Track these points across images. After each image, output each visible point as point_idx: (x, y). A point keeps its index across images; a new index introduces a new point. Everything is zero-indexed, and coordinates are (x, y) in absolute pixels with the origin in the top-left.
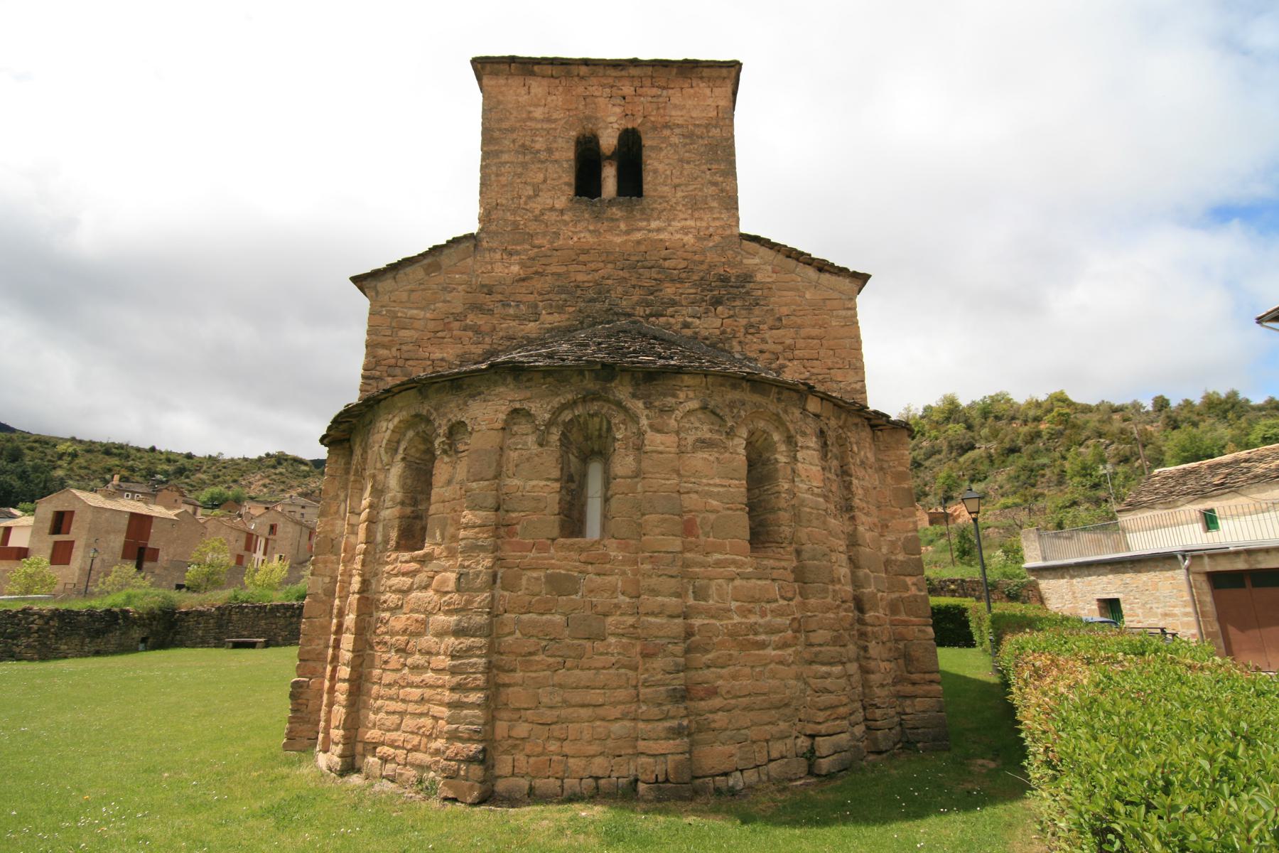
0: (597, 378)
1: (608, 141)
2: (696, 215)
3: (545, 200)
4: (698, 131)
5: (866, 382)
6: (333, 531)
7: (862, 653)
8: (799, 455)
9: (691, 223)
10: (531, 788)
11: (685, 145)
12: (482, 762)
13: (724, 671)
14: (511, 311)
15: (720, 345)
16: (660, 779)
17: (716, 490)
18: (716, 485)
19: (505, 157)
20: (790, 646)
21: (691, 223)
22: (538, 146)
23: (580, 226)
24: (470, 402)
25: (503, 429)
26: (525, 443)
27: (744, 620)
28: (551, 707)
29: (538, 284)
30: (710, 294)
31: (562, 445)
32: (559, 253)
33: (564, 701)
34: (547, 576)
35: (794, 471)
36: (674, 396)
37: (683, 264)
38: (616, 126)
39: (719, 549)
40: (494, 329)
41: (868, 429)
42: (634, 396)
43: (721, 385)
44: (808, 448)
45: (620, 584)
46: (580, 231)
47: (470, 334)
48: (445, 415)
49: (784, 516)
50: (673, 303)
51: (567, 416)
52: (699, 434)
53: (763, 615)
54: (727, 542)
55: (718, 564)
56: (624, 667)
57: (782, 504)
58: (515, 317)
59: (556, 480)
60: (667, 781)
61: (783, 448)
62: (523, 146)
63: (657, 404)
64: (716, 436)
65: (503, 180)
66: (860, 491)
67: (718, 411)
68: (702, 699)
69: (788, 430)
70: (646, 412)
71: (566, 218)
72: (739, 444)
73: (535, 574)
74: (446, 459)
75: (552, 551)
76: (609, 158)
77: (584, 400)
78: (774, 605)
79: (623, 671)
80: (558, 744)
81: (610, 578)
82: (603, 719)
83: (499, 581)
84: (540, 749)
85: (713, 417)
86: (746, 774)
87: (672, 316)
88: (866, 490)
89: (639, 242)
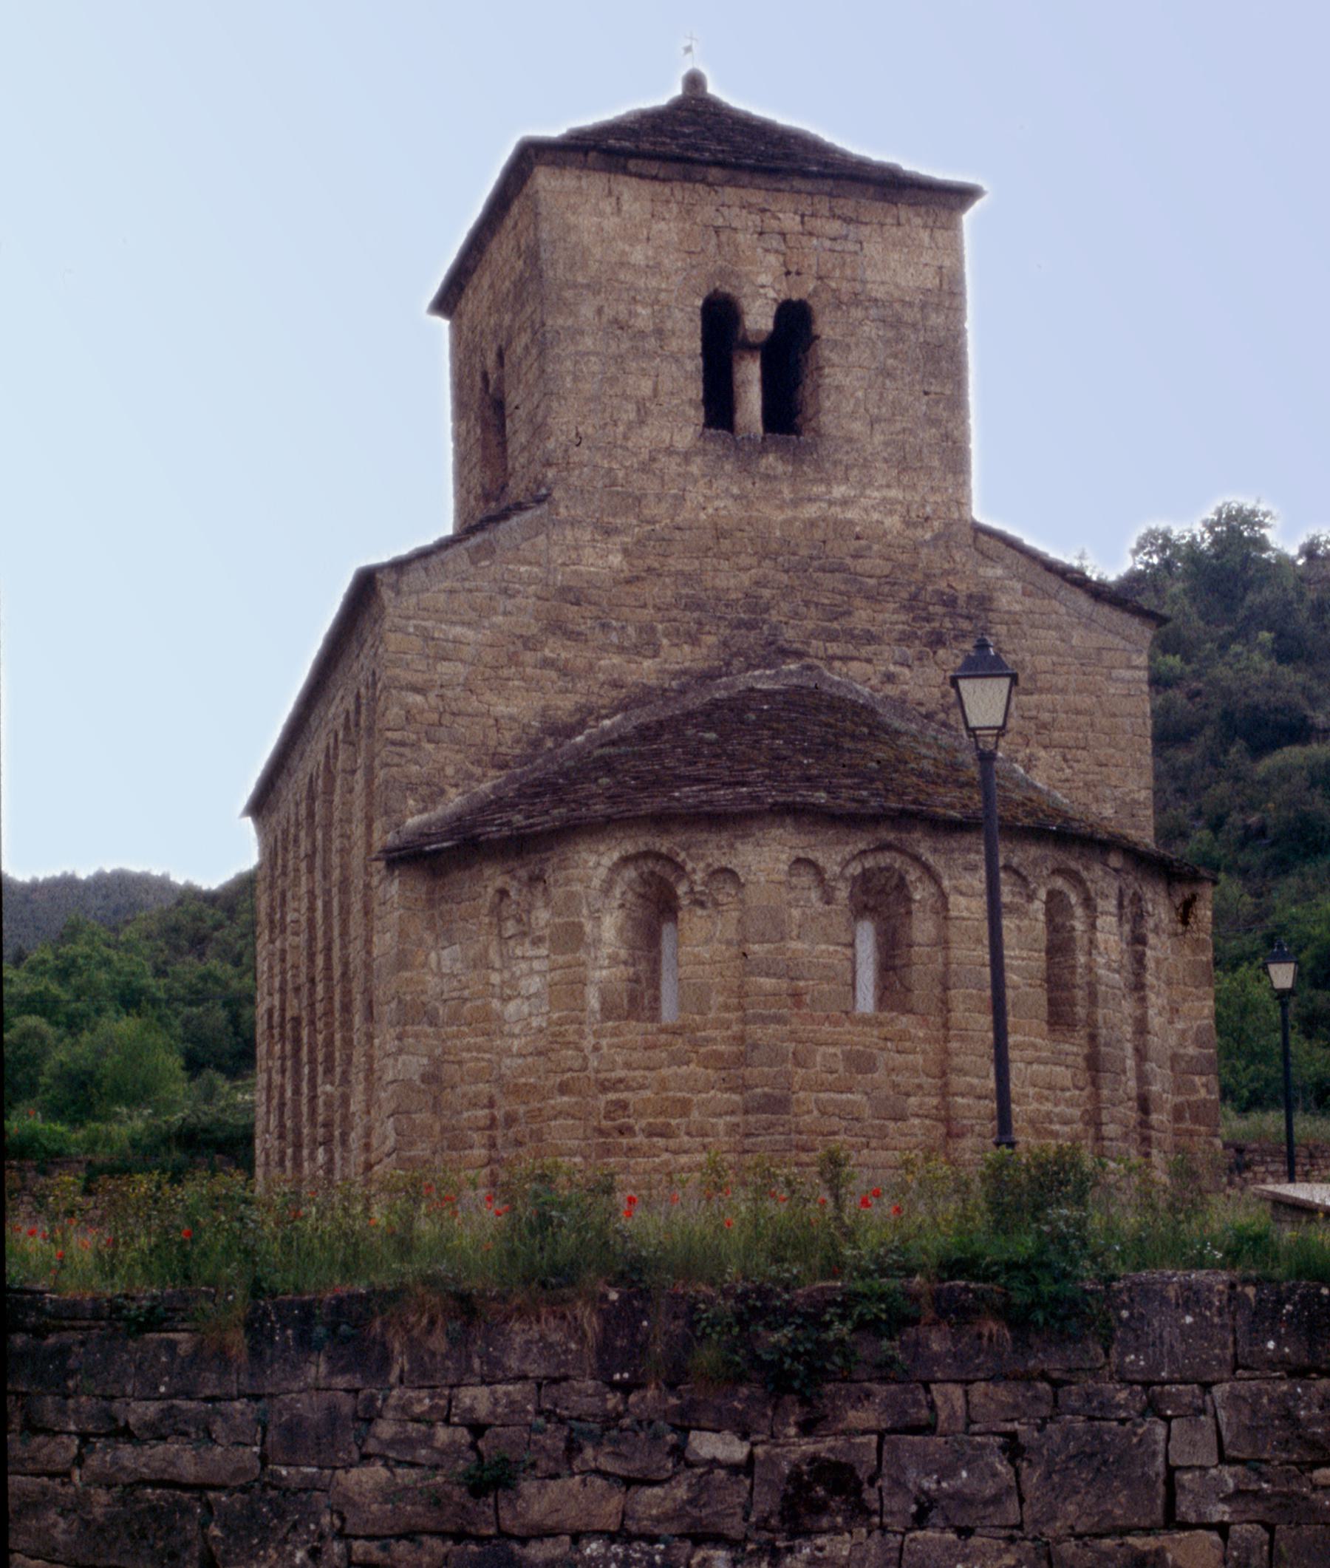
1: (759, 318)
2: (905, 479)
3: (648, 436)
4: (911, 315)
6: (424, 992)
8: (1099, 923)
9: (894, 493)
11: (887, 342)
14: (614, 638)
19: (588, 342)
21: (894, 493)
22: (639, 323)
23: (721, 483)
24: (738, 845)
26: (808, 900)
29: (653, 591)
30: (928, 627)
32: (687, 535)
35: (1091, 942)
37: (886, 568)
38: (772, 294)
40: (591, 666)
42: (935, 851)
46: (712, 494)
47: (554, 675)
48: (702, 857)
50: (871, 638)
51: (855, 869)
57: (1078, 981)
58: (621, 649)
61: (1079, 911)
62: (615, 321)
65: (588, 387)
71: (694, 469)
72: (1038, 906)
76: (751, 348)
87: (869, 661)
88: (1158, 962)
89: (812, 524)
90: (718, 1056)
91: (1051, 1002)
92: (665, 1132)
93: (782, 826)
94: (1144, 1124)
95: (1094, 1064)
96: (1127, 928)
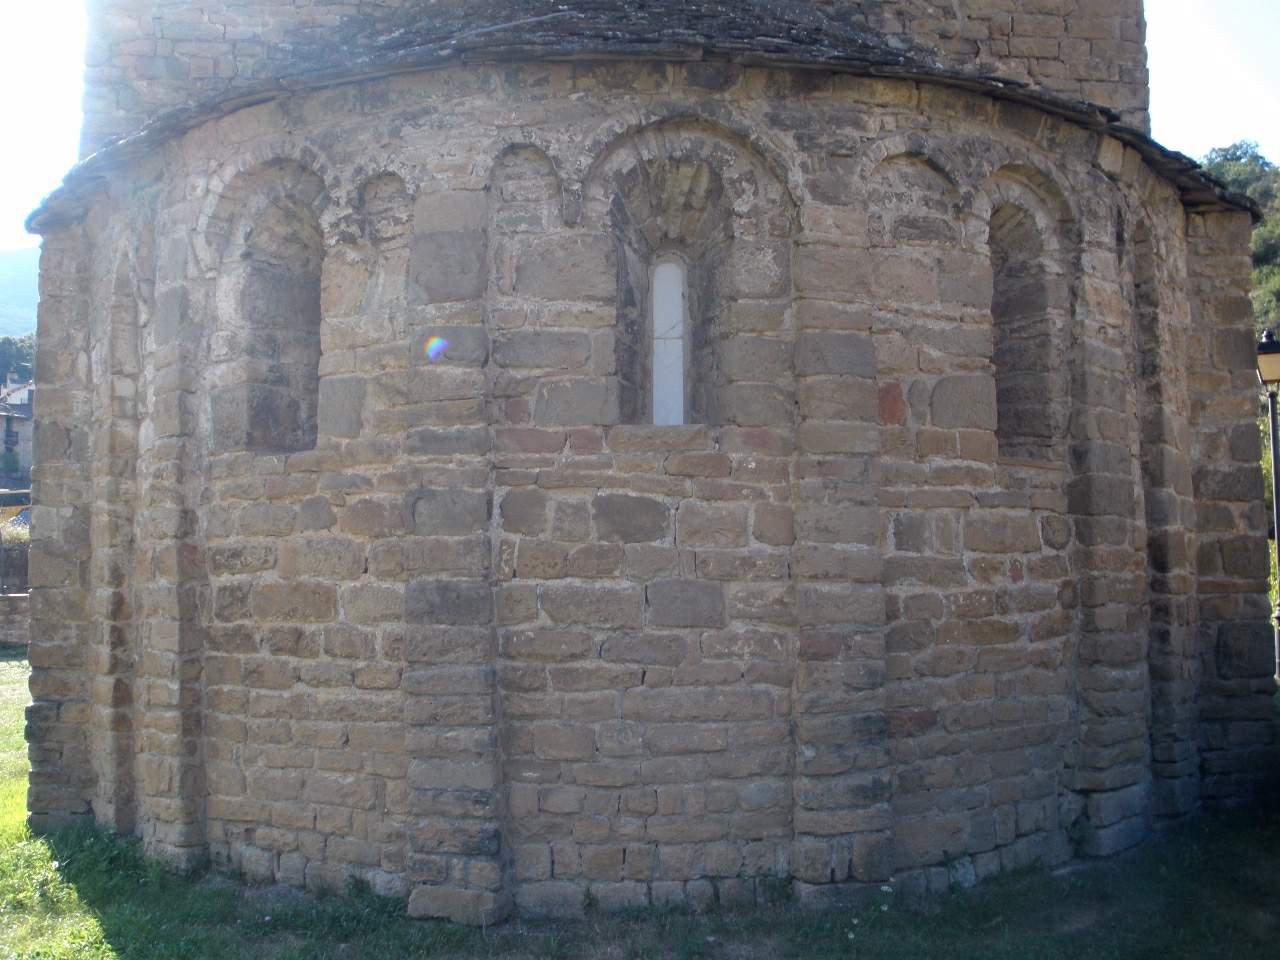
0: (693, 80)
5: (1153, 110)
7: (1156, 645)
8: (1086, 259)
10: (588, 894)
12: (494, 855)
13: (948, 681)
15: (858, 18)
16: (839, 875)
17: (932, 324)
18: (938, 317)
20: (1058, 634)
25: (487, 189)
26: (535, 220)
27: (984, 586)
28: (622, 757)
31: (614, 225)
33: (647, 745)
34: (599, 503)
35: (1074, 293)
36: (858, 124)
39: (941, 445)
41: (1180, 209)
42: (774, 121)
43: (947, 106)
44: (1099, 245)
45: (752, 520)
48: (347, 158)
49: (1057, 381)
51: (623, 160)
52: (906, 208)
53: (1016, 576)
54: (956, 432)
55: (941, 475)
56: (765, 679)
59: (609, 301)
60: (850, 878)
61: (1053, 244)
63: (823, 140)
64: (935, 214)
66: (1167, 337)
67: (941, 160)
68: (910, 735)
69: (1065, 207)
70: (800, 157)
72: (976, 230)
73: (573, 497)
74: (352, 255)
75: (606, 451)
77: (659, 126)
78: (1035, 557)
79: (762, 686)
80: (639, 822)
81: (731, 505)
82: (726, 776)
83: (496, 511)
84: (604, 832)
85: (930, 173)
86: (982, 859)
90: (371, 509)
91: (1003, 396)
92: (297, 643)
93: (484, 89)
94: (1158, 586)
95: (1080, 499)
96: (1128, 277)
